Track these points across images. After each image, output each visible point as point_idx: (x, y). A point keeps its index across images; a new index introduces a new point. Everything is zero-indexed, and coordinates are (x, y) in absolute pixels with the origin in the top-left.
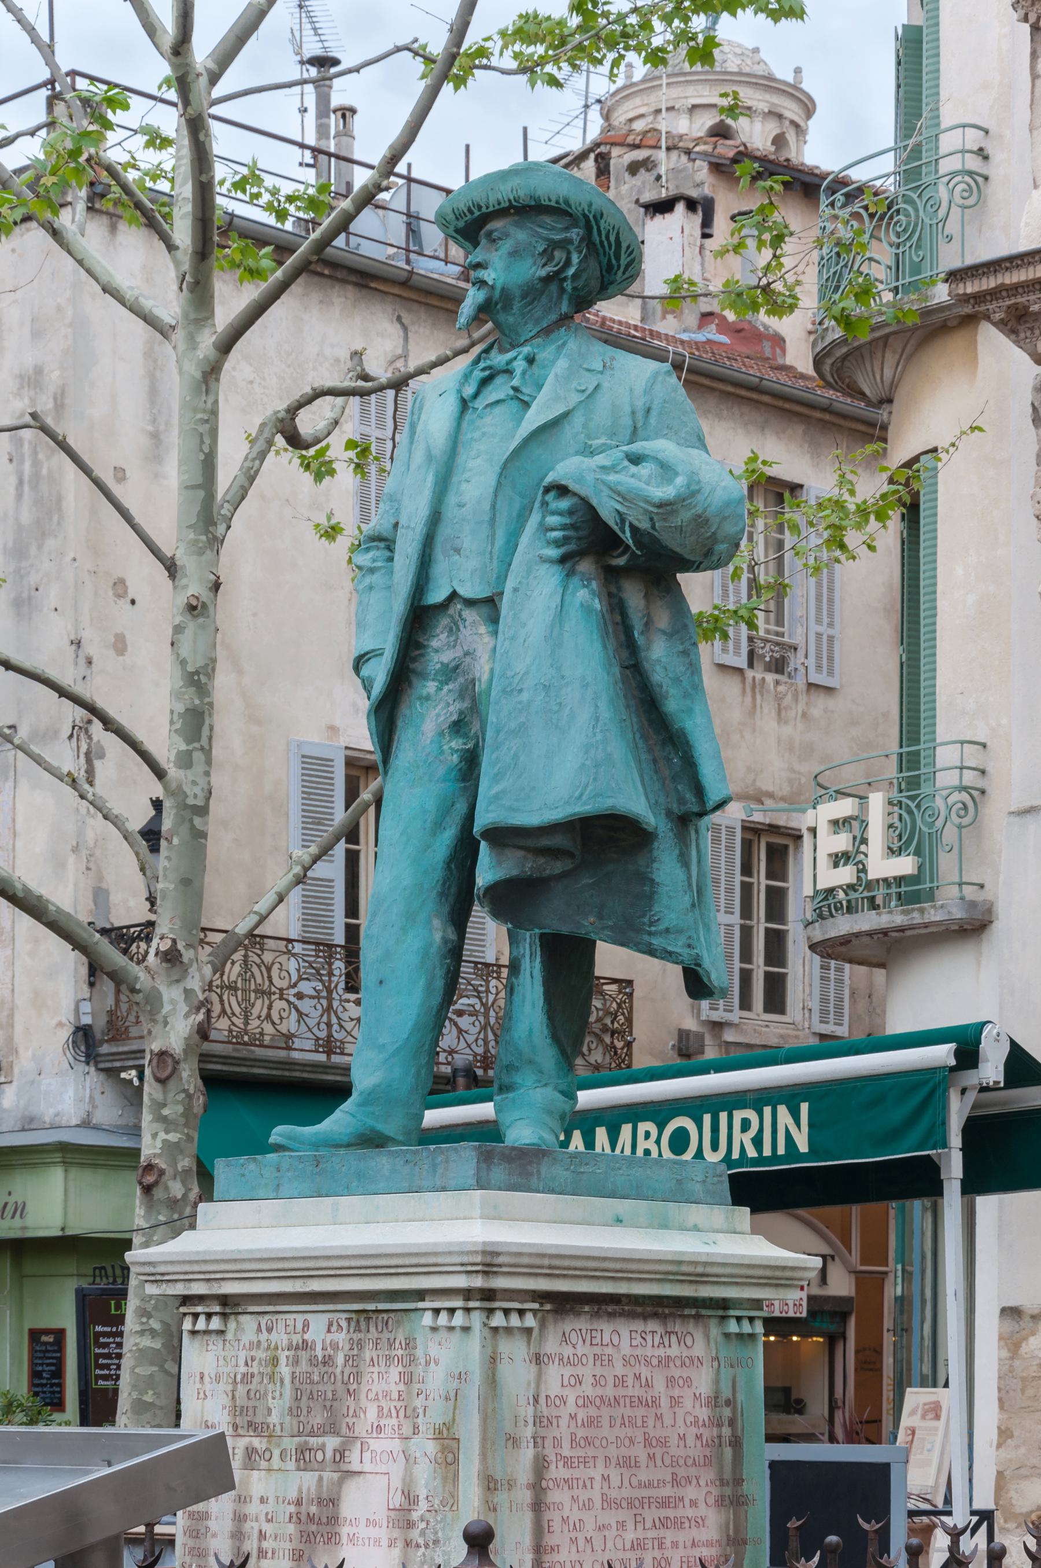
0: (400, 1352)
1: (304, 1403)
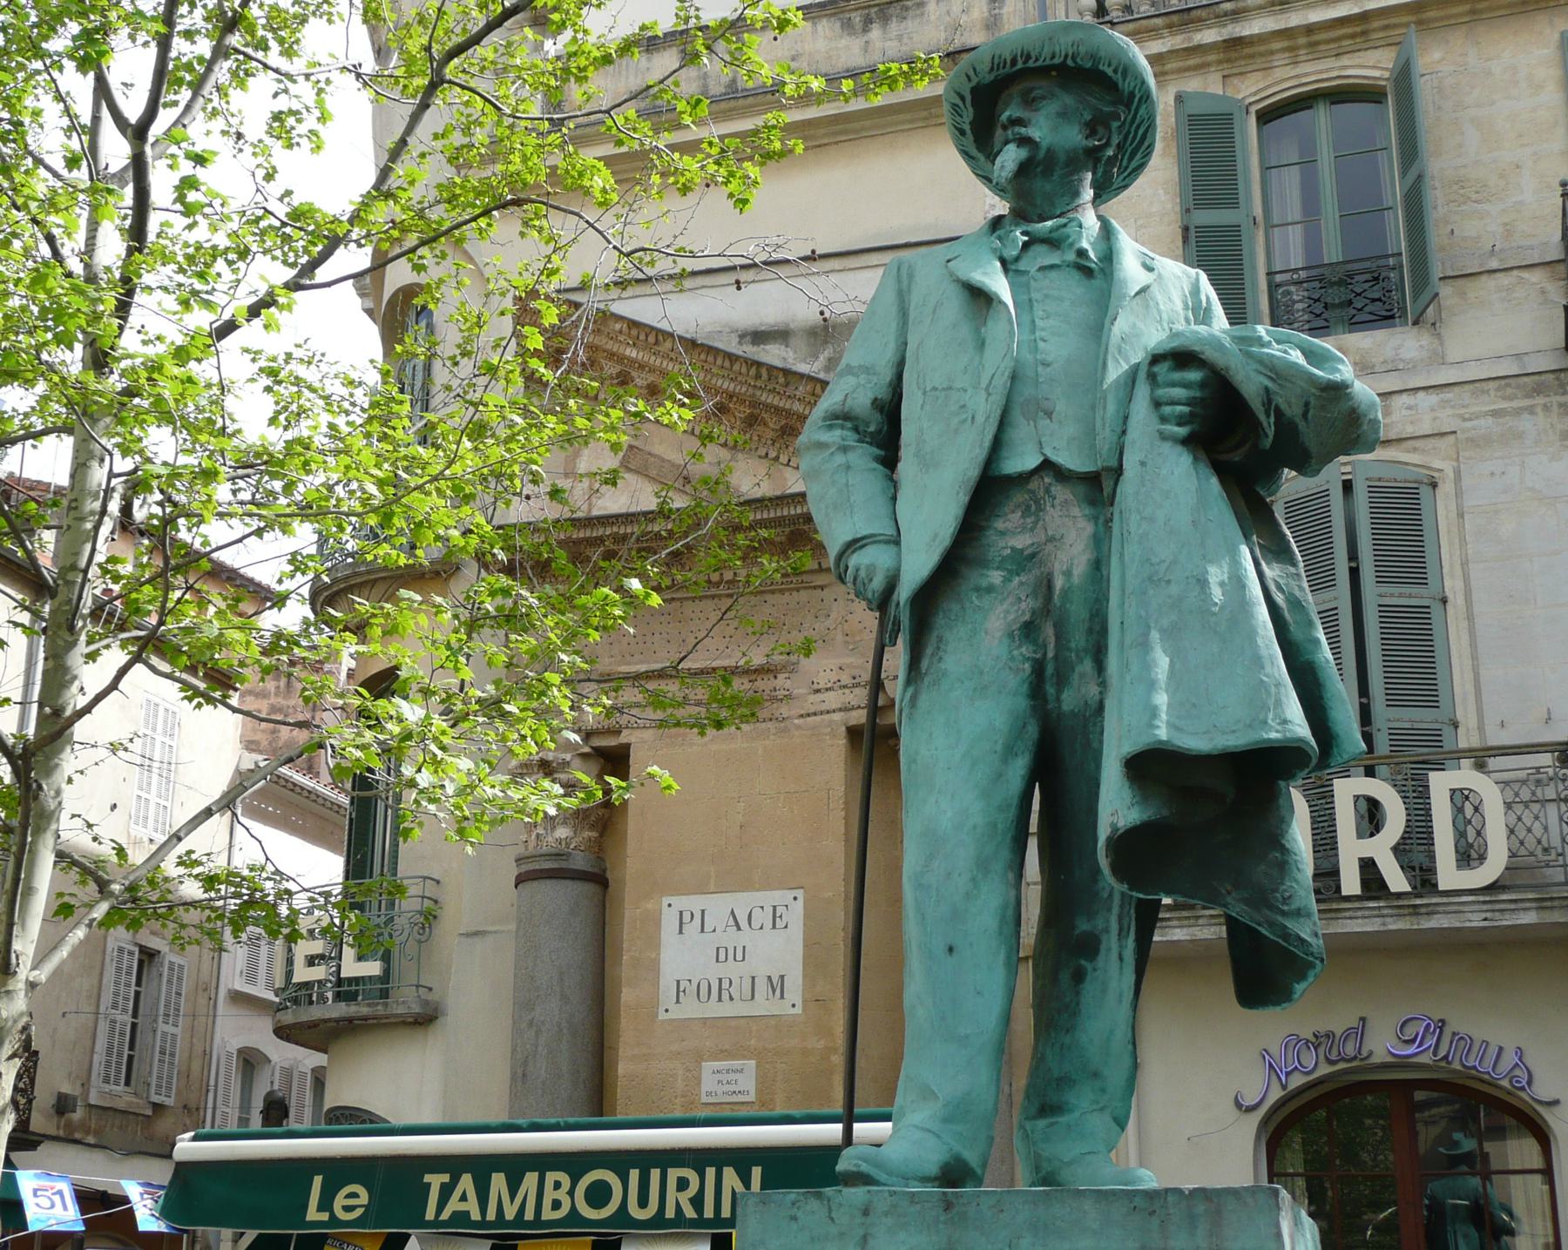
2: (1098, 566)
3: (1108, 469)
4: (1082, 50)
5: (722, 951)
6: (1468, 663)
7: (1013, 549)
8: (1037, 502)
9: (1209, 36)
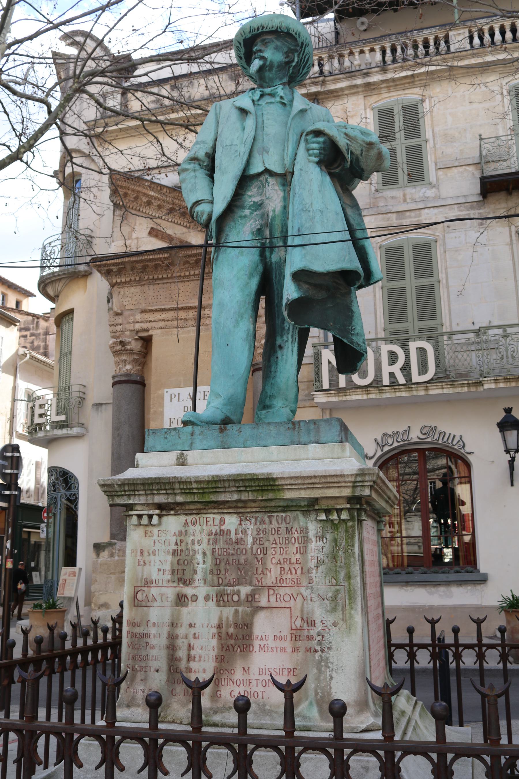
0: (296, 535)
1: (222, 567)
2: (285, 208)
3: (290, 172)
4: (283, 25)
5: (186, 408)
6: (446, 303)
7: (254, 202)
8: (263, 185)
9: (359, 81)
